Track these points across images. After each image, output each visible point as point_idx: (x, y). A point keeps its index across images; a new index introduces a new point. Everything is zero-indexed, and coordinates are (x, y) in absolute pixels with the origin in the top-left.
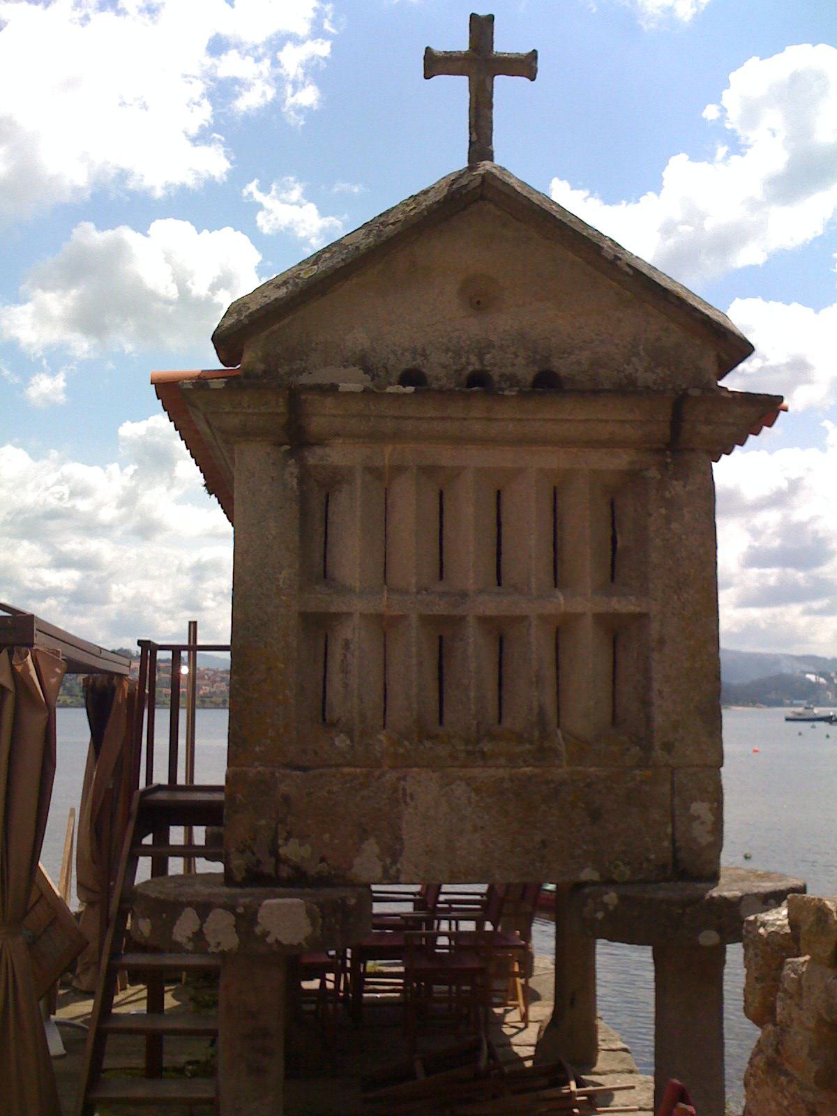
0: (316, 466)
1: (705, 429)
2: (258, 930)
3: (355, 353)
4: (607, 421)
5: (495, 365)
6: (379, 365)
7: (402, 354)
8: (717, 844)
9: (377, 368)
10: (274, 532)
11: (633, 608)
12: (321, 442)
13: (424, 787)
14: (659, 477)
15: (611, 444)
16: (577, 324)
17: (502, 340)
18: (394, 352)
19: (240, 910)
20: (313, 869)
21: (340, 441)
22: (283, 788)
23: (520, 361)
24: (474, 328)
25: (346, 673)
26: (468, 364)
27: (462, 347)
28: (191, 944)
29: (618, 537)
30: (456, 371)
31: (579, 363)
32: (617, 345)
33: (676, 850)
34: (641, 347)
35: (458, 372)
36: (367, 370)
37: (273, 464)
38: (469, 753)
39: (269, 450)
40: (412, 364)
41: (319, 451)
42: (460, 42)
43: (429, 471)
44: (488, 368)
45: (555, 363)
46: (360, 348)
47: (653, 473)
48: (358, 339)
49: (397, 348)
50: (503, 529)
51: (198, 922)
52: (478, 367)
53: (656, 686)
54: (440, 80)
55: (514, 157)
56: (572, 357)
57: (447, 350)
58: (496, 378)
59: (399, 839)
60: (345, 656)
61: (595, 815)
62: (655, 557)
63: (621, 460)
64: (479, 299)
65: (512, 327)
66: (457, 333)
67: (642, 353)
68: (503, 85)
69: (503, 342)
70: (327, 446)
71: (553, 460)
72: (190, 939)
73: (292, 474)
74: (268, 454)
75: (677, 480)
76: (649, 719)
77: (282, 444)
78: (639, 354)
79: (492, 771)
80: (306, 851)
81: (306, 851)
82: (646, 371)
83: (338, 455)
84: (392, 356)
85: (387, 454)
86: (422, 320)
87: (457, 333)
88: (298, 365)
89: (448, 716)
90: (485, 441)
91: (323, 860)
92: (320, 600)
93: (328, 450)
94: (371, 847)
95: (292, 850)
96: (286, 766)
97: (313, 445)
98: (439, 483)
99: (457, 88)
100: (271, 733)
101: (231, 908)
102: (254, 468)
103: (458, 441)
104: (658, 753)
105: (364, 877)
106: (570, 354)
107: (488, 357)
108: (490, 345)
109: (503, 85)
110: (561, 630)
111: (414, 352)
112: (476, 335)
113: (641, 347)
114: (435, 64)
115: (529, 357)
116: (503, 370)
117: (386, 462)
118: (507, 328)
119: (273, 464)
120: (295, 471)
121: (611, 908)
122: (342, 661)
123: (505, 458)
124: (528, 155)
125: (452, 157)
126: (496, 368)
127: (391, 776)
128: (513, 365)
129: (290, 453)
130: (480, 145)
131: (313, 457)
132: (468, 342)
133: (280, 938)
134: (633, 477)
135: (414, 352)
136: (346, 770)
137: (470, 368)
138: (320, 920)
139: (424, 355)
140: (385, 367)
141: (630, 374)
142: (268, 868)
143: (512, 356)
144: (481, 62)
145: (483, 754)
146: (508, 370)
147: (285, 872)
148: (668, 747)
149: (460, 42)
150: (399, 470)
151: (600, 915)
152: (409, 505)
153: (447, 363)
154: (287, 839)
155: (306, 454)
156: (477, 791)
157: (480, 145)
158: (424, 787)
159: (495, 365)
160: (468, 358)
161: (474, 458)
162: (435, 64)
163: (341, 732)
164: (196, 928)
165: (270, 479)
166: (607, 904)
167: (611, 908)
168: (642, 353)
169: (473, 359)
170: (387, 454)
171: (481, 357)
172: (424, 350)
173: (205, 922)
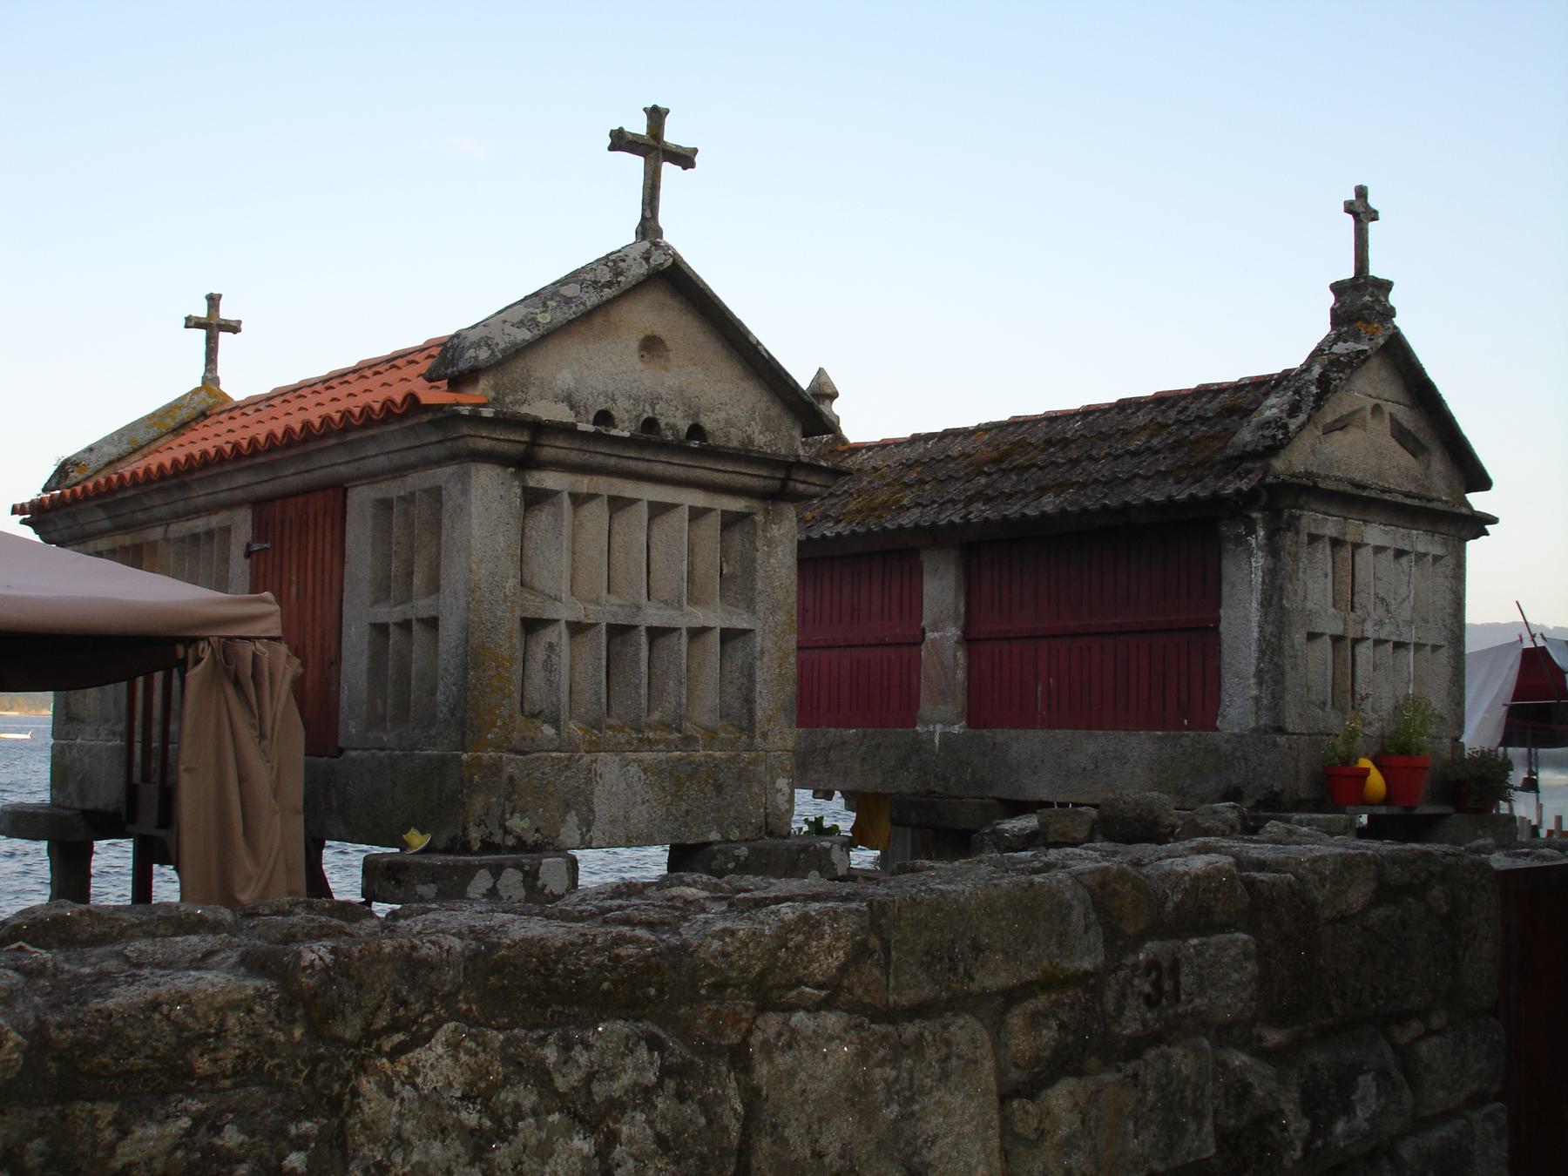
2: (540, 883)
8: (790, 811)
11: (745, 626)
13: (609, 767)
19: (527, 868)
20: (531, 838)
22: (509, 770)
23: (679, 414)
33: (767, 815)
35: (638, 417)
36: (572, 407)
38: (641, 740)
40: (604, 407)
42: (638, 126)
48: (565, 379)
53: (758, 687)
55: (679, 234)
58: (663, 426)
59: (592, 811)
61: (719, 789)
62: (760, 585)
68: (224, 337)
72: (1299, 518)
76: (751, 713)
79: (654, 755)
80: (525, 823)
81: (525, 823)
86: (599, 375)
88: (520, 396)
89: (616, 708)
91: (537, 830)
92: (535, 607)
94: (572, 819)
95: (517, 823)
96: (511, 751)
99: (634, 165)
100: (499, 723)
101: (518, 866)
104: (758, 740)
105: (568, 842)
108: (659, 398)
109: (224, 337)
124: (692, 237)
125: (620, 233)
127: (587, 758)
136: (554, 754)
137: (645, 416)
139: (614, 400)
142: (497, 839)
144: (652, 147)
145: (649, 740)
146: (671, 420)
147: (510, 841)
148: (764, 736)
150: (591, 497)
154: (512, 813)
156: (645, 771)
158: (609, 767)
169: (648, 408)
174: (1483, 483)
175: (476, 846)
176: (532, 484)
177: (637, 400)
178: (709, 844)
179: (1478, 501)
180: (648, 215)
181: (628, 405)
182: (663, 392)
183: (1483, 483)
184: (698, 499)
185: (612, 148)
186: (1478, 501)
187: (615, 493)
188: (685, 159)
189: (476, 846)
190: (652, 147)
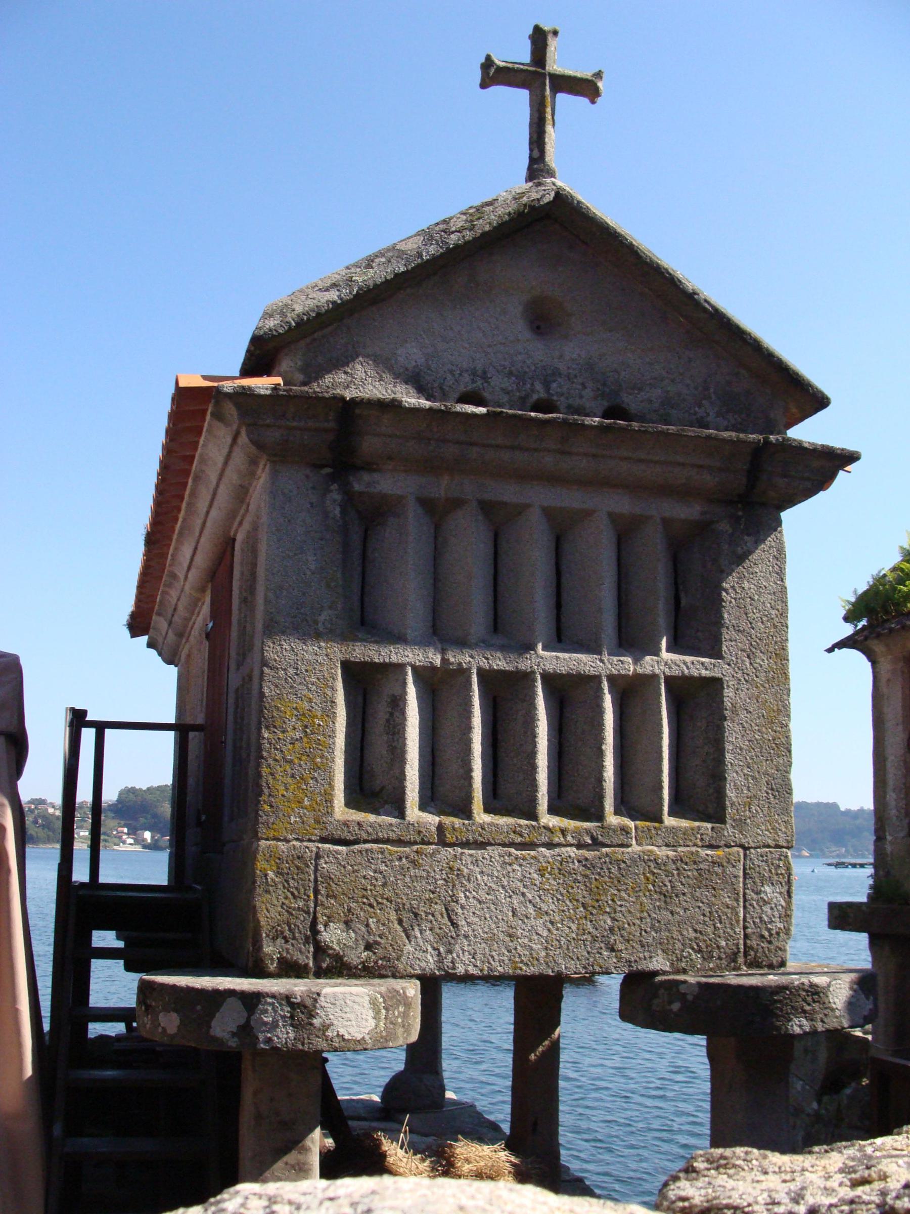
0: (361, 494)
1: (781, 482)
3: (407, 370)
4: (683, 465)
5: (562, 395)
6: (436, 385)
7: (460, 375)
9: (432, 388)
10: (313, 567)
12: (369, 467)
14: (730, 531)
15: (684, 493)
16: (648, 360)
17: (568, 368)
18: (452, 372)
21: (390, 467)
23: (588, 393)
24: (537, 352)
25: (394, 734)
26: (533, 391)
27: (525, 372)
28: (236, 1039)
29: (682, 595)
30: (521, 398)
31: (650, 401)
32: (688, 385)
34: (712, 390)
37: (313, 488)
39: (308, 472)
40: (470, 387)
41: (366, 477)
42: (519, 53)
43: (488, 508)
44: (555, 398)
45: (625, 399)
46: (414, 364)
47: (724, 526)
49: (454, 368)
50: (563, 580)
51: (246, 1014)
52: (543, 395)
54: (500, 92)
56: (643, 394)
57: (511, 373)
60: (391, 714)
63: (687, 512)
64: (542, 320)
65: (579, 355)
66: (520, 357)
67: (713, 397)
68: (566, 105)
69: (571, 371)
70: (375, 471)
71: (622, 504)
72: (234, 1034)
73: (335, 501)
74: (307, 476)
75: (749, 535)
77: (322, 466)
78: (710, 398)
82: (717, 416)
83: (387, 483)
84: (449, 377)
85: (442, 487)
87: (520, 357)
90: (554, 479)
93: (376, 476)
97: (362, 468)
98: (499, 520)
102: (291, 491)
103: (524, 476)
106: (640, 389)
107: (554, 385)
108: (556, 373)
110: (630, 692)
111: (474, 373)
112: (542, 361)
113: (712, 390)
114: (494, 75)
115: (598, 389)
116: (571, 401)
117: (443, 493)
118: (575, 356)
119: (313, 488)
120: (337, 497)
121: (690, 998)
122: (388, 721)
123: (570, 499)
124: (596, 169)
126: (562, 399)
128: (581, 397)
129: (332, 478)
130: (537, 167)
131: (360, 484)
132: (533, 368)
133: (342, 1031)
134: (703, 528)
135: (474, 373)
137: (535, 397)
138: (383, 1011)
139: (485, 377)
140: (441, 388)
141: (702, 417)
143: (580, 387)
144: (538, 78)
149: (519, 53)
150: (456, 503)
151: (676, 1006)
152: (469, 543)
153: (510, 388)
155: (351, 478)
157: (537, 167)
159: (562, 395)
160: (532, 385)
161: (541, 497)
162: (494, 75)
163: (386, 802)
164: (242, 1021)
165: (309, 506)
166: (685, 994)
167: (690, 998)
168: (713, 397)
169: (538, 386)
170: (442, 487)
171: (547, 385)
172: (485, 372)
173: (253, 1013)
174: (816, 402)
175: (273, 967)
176: (357, 487)
177: (521, 378)
178: (655, 973)
179: (808, 432)
180: (536, 154)
181: (508, 383)
182: (562, 367)
183: (816, 402)
184: (622, 504)
185: (484, 85)
186: (808, 432)
187: (488, 497)
188: (586, 88)
189: (273, 967)
190: (538, 78)
